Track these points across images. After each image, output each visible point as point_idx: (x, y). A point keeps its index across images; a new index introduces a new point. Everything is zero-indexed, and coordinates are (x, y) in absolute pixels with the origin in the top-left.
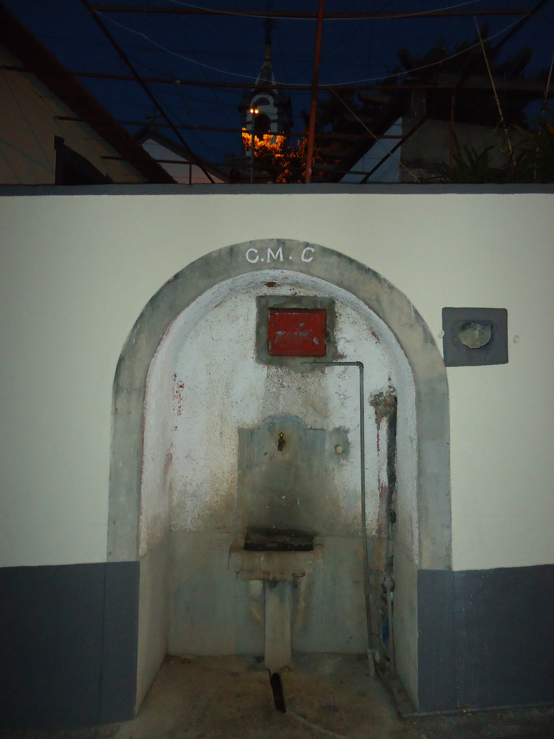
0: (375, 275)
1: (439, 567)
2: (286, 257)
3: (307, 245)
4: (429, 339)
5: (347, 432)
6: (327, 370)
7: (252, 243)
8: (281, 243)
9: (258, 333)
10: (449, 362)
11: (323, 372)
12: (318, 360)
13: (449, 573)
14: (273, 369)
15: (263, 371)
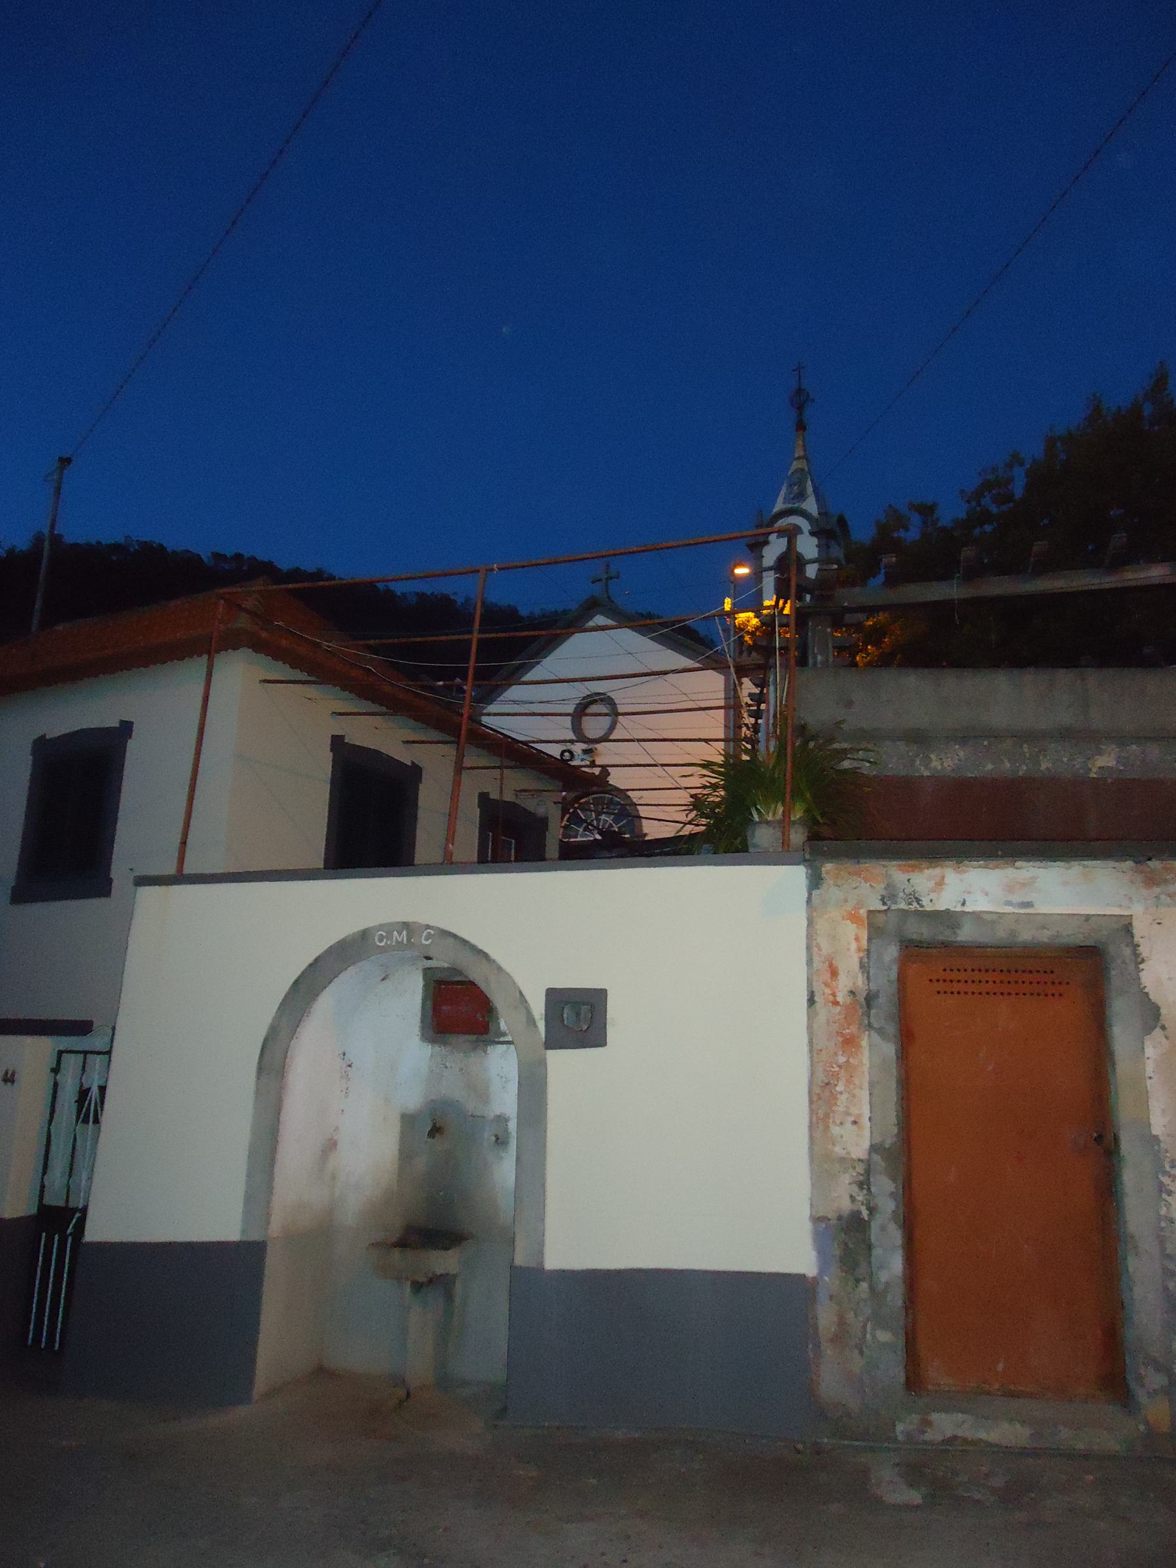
0: (486, 956)
1: (533, 1264)
2: (409, 940)
3: (428, 927)
4: (531, 1021)
5: (507, 1120)
6: (490, 1049)
7: (381, 927)
8: (406, 925)
9: (423, 1008)
10: (553, 1043)
11: (485, 1052)
12: (480, 1037)
13: (540, 1269)
14: (437, 1048)
15: (427, 1050)
